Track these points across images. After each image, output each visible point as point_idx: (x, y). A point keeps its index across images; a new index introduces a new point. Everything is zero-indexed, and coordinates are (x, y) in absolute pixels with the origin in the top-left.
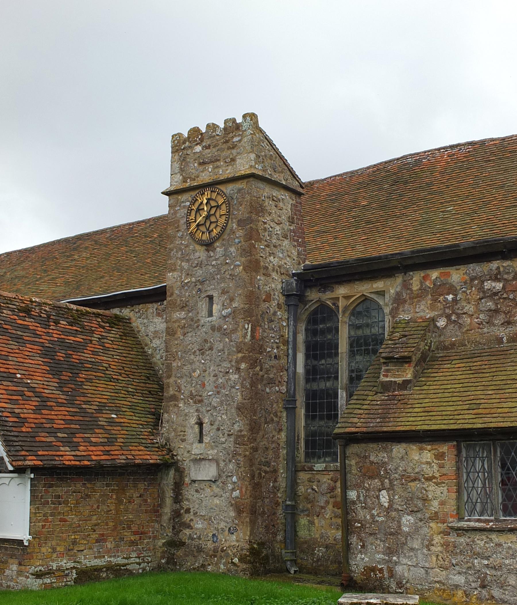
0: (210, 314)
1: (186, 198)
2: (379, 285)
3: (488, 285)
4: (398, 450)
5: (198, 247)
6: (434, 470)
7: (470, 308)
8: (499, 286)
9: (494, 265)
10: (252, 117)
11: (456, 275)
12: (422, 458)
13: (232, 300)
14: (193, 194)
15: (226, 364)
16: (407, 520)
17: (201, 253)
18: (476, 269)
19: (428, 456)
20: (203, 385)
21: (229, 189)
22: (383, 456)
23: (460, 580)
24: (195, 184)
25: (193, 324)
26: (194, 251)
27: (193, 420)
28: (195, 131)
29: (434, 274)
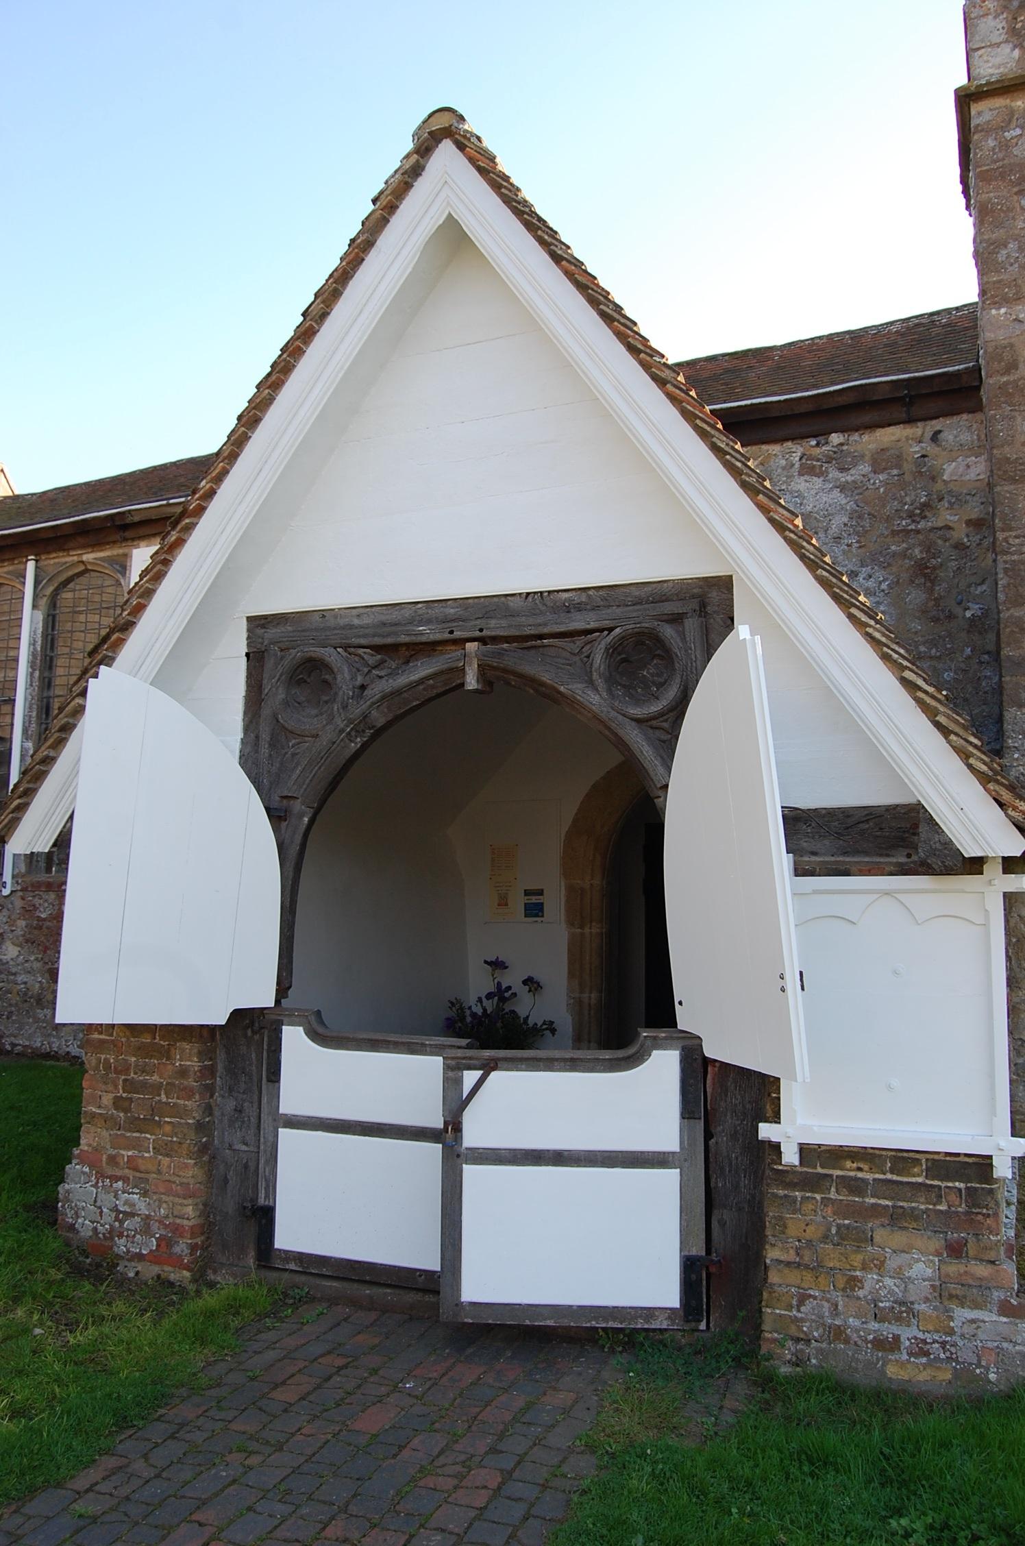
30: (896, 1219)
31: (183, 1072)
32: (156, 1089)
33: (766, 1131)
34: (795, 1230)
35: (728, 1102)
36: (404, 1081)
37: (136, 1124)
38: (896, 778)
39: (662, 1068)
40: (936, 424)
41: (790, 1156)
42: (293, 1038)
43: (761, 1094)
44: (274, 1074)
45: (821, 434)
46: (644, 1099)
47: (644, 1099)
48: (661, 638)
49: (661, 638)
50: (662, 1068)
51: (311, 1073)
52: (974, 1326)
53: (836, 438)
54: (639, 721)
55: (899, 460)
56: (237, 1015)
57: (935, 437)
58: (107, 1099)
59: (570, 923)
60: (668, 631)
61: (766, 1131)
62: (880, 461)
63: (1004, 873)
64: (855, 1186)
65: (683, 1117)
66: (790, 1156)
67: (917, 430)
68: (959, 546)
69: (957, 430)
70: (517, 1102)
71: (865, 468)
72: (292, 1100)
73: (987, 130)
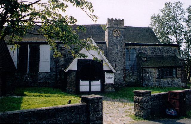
0: (117, 48)
1: (112, 29)
2: (136, 47)
3: (151, 49)
4: (150, 69)
5: (115, 37)
6: (154, 72)
7: (149, 51)
8: (152, 49)
9: (152, 46)
10: (123, 20)
11: (147, 47)
12: (153, 70)
13: (122, 46)
14: (113, 29)
15: (121, 56)
16: (151, 78)
17: (115, 38)
18: (150, 47)
19: (153, 70)
20: (116, 59)
21: (121, 29)
22: (148, 70)
23: (157, 84)
24: (147, 43)
25: (114, 49)
26: (114, 38)
27: (115, 64)
28: (112, 19)
29: (144, 46)
57: (103, 45)
67: (102, 45)
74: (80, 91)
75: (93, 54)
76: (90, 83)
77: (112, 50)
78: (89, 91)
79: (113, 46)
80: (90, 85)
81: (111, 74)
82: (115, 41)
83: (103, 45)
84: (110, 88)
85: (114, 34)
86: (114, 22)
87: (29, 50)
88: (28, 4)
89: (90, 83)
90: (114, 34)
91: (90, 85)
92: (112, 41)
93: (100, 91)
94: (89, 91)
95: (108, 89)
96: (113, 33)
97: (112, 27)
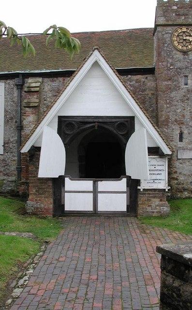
17: (179, 56)
20: (184, 116)
25: (177, 88)
27: (178, 132)
30: (154, 197)
31: (49, 186)
32: (44, 188)
33: (139, 187)
34: (141, 199)
35: (133, 184)
36: (88, 184)
37: (40, 194)
38: (156, 143)
39: (124, 180)
40: (147, 76)
41: (142, 190)
42: (67, 180)
43: (137, 182)
44: (64, 186)
45: (127, 75)
46: (121, 185)
47: (121, 185)
48: (127, 125)
49: (127, 125)
50: (124, 180)
51: (70, 184)
52: (120, 255)
53: (129, 76)
54: (121, 135)
55: (140, 82)
56: (60, 176)
57: (146, 78)
58: (34, 191)
59: (79, 162)
60: (126, 123)
61: (139, 187)
62: (137, 81)
63: (149, 148)
64: (150, 194)
65: (127, 187)
66: (142, 190)
67: (143, 76)
68: (150, 98)
69: (150, 77)
70: (103, 185)
71: (134, 82)
72: (67, 188)
73: (158, 31)
74: (67, 208)
75: (96, 95)
76: (95, 187)
77: (170, 89)
78: (92, 209)
79: (176, 78)
80: (95, 192)
81: (159, 159)
82: (179, 65)
83: (146, 78)
84: (156, 202)
85: (175, 43)
86: (175, 8)
87: (56, 71)
88: (165, 153)
89: (95, 187)
90: (175, 43)
91: (95, 192)
92: (171, 65)
93: (125, 209)
94: (92, 209)
95: (149, 206)
96: (172, 41)
97: (170, 23)
